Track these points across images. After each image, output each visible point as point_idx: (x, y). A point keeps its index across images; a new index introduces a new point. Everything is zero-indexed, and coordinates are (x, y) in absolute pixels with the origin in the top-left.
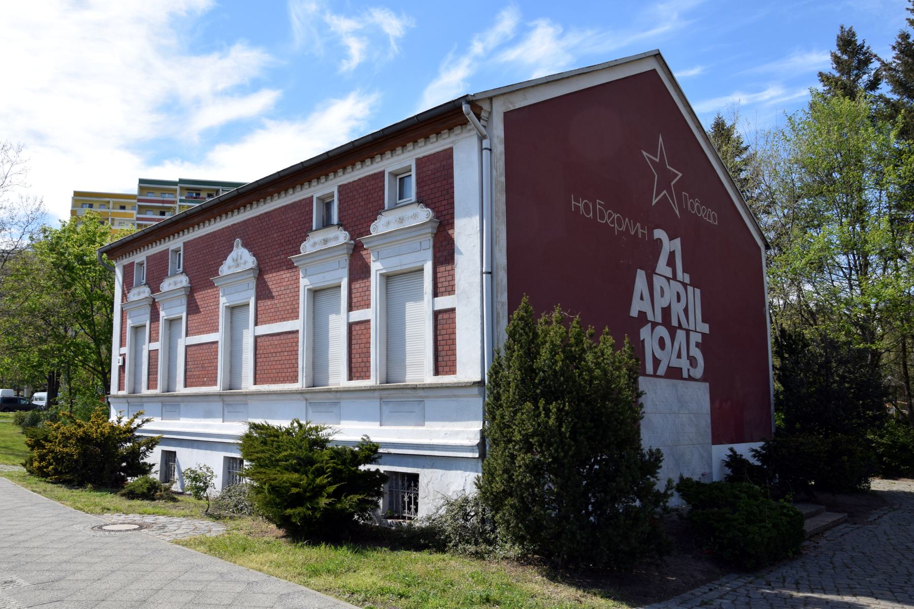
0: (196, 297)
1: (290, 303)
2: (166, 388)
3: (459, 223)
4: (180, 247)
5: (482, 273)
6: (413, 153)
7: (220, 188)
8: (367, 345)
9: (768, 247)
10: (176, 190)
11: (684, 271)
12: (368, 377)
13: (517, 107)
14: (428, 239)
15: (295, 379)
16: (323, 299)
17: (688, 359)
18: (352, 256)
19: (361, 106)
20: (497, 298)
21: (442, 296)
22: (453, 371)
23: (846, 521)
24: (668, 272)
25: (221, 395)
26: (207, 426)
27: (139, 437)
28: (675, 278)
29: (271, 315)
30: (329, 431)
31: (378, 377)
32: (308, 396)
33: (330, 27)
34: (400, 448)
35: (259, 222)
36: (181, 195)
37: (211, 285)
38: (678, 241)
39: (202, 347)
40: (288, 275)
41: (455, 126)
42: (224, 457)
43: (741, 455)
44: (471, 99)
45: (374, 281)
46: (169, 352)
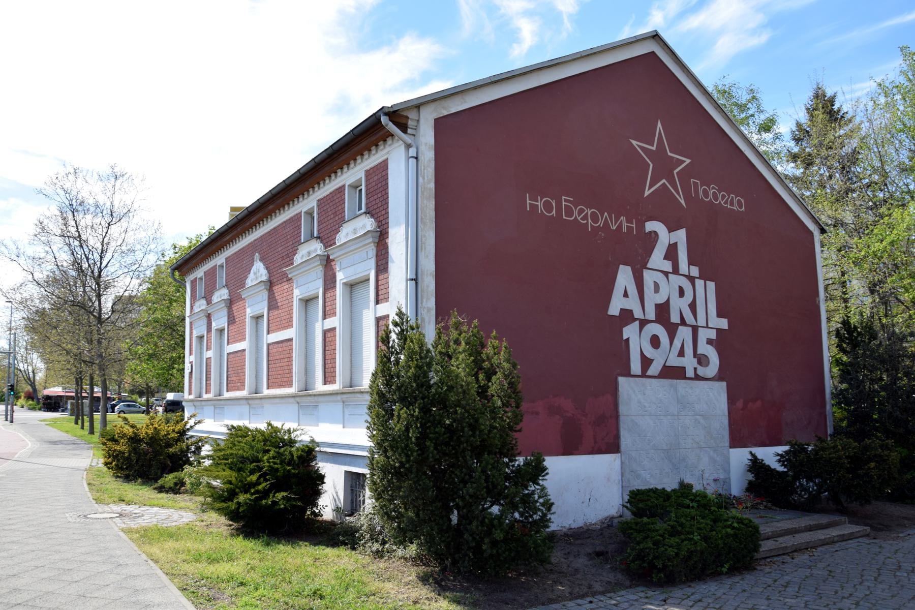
3: (392, 231)
5: (407, 280)
9: (823, 231)
11: (691, 263)
13: (453, 111)
15: (290, 384)
20: (421, 303)
21: (382, 303)
23: (868, 535)
24: (668, 266)
25: (246, 399)
28: (676, 270)
34: (342, 449)
39: (237, 355)
43: (762, 460)
44: (387, 110)
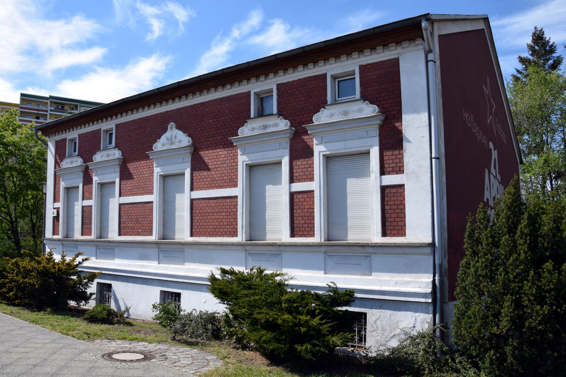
0: (129, 167)
2: (99, 235)
3: (407, 119)
4: (76, 137)
5: (431, 159)
6: (358, 60)
7: (79, 104)
10: (47, 103)
12: (313, 235)
16: (171, 183)
18: (193, 155)
19: (160, 63)
25: (157, 243)
26: (144, 266)
27: (80, 271)
29: (208, 183)
30: (286, 277)
32: (248, 248)
33: (139, 11)
35: (194, 110)
36: (51, 106)
37: (147, 158)
40: (225, 152)
41: (403, 41)
42: (161, 291)
45: (318, 161)
46: (101, 208)
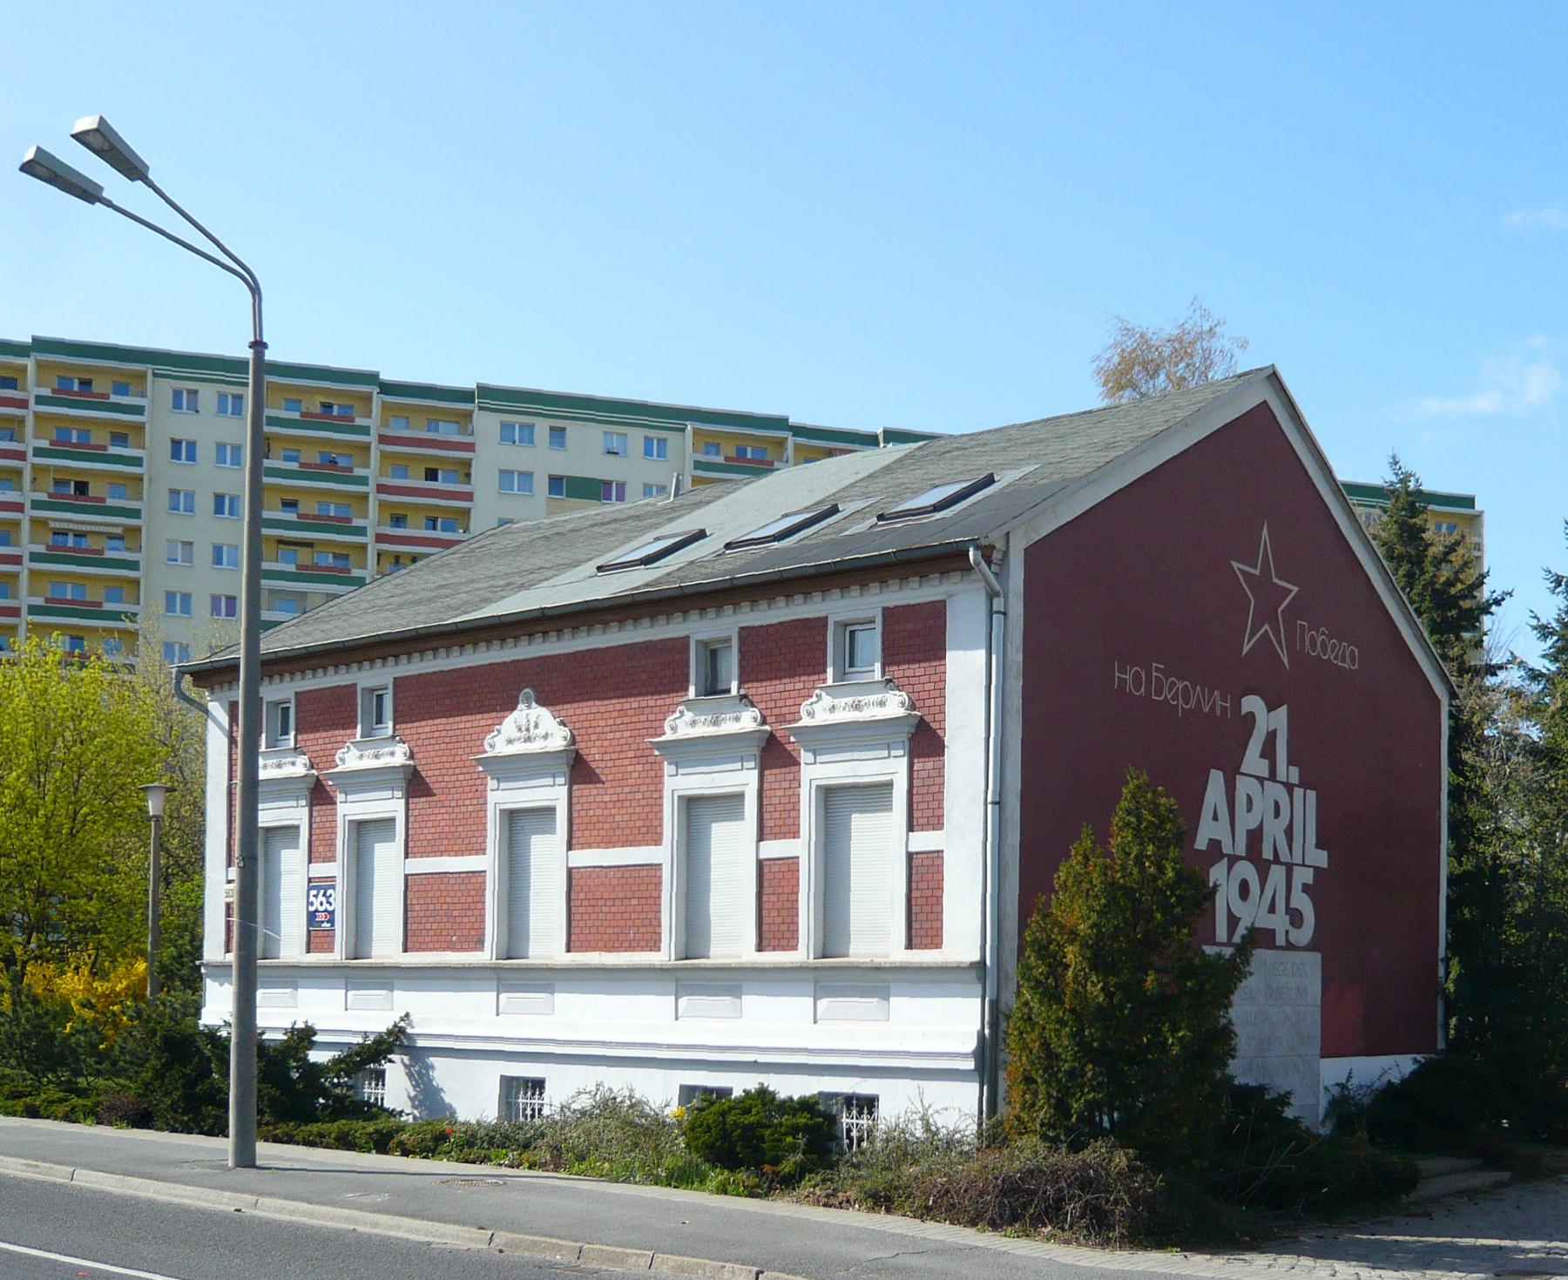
1: (643, 816)
8: (793, 897)
14: (902, 739)
17: (1287, 913)
22: (937, 945)
24: (1262, 768)
28: (1273, 776)
31: (811, 949)
38: (1282, 712)
